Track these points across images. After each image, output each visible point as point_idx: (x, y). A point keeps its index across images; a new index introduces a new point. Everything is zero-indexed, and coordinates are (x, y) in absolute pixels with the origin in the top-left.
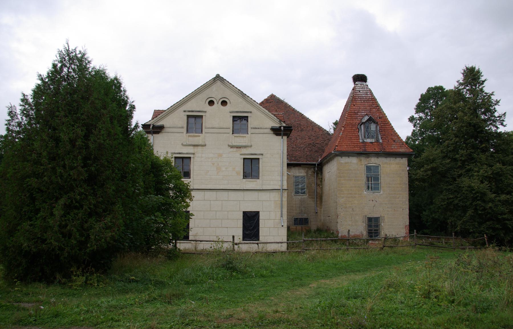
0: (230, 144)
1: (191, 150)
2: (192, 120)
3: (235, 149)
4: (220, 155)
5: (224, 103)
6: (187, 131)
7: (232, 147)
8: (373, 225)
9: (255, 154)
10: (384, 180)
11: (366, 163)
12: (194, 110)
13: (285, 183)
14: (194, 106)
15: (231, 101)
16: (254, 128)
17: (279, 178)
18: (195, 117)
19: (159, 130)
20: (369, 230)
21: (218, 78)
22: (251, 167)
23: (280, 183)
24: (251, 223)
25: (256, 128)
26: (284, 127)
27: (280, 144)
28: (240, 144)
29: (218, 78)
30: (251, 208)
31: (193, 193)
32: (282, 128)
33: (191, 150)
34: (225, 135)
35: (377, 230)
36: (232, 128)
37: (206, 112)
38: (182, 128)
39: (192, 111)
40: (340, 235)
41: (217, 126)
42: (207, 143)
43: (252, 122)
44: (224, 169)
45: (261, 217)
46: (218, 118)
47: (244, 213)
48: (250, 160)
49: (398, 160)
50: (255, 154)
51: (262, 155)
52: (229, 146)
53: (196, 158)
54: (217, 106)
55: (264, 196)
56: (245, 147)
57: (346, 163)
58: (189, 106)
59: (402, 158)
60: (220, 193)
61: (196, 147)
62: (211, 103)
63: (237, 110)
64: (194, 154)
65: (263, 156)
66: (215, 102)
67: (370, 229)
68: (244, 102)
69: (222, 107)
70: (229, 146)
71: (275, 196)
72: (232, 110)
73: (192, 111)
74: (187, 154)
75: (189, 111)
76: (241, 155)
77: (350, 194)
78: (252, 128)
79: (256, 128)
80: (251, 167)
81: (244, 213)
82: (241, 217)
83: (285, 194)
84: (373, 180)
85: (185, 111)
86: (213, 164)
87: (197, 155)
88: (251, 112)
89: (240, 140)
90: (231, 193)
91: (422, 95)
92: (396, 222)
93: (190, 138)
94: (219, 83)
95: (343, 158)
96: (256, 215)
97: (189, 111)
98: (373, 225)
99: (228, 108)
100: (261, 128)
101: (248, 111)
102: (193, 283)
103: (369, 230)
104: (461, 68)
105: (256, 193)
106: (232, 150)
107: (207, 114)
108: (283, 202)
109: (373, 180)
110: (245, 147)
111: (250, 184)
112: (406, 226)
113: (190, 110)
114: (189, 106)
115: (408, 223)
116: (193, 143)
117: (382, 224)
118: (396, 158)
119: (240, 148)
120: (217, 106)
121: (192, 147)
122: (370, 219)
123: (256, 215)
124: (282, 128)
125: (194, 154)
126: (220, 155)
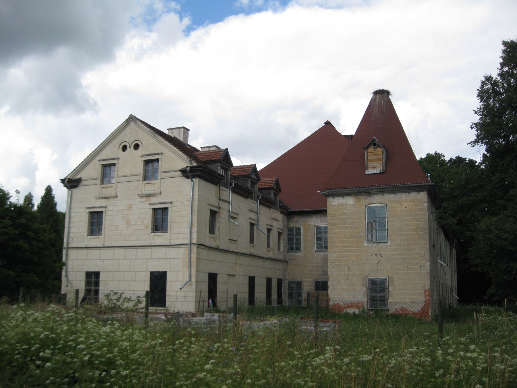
0: (140, 193)
1: (103, 203)
3: (144, 199)
4: (130, 207)
7: (142, 196)
8: (378, 290)
9: (164, 203)
11: (367, 202)
12: (108, 158)
13: (195, 236)
14: (107, 154)
15: (143, 143)
17: (188, 230)
19: (75, 184)
20: (372, 297)
21: (132, 119)
22: (160, 219)
23: (188, 237)
25: (166, 172)
28: (150, 192)
29: (132, 119)
30: (159, 268)
33: (103, 203)
34: (93, 187)
35: (384, 297)
37: (118, 159)
38: (97, 179)
39: (106, 160)
40: (331, 303)
42: (118, 194)
43: (163, 165)
44: (133, 222)
46: (131, 163)
47: (152, 273)
48: (161, 211)
49: (414, 195)
50: (164, 203)
52: (138, 195)
53: (107, 212)
54: (130, 150)
55: (173, 252)
56: (155, 195)
57: (339, 205)
58: (103, 155)
59: (418, 192)
60: (117, 251)
61: (108, 200)
62: (124, 148)
63: (148, 153)
65: (173, 205)
66: (128, 147)
67: (373, 294)
69: (134, 151)
70: (138, 195)
71: (183, 252)
73: (106, 160)
74: (100, 207)
75: (103, 160)
76: (150, 204)
79: (166, 172)
80: (160, 219)
81: (152, 273)
82: (148, 279)
84: (376, 224)
85: (100, 161)
86: (123, 217)
87: (108, 208)
88: (162, 154)
89: (150, 188)
90: (140, 251)
91: (488, 91)
92: (411, 287)
93: (104, 190)
94: (132, 124)
95: (336, 198)
96: (97, 275)
97: (103, 160)
98: (378, 290)
99: (140, 151)
100: (172, 171)
101: (159, 152)
103: (372, 297)
104: (501, 43)
105: (164, 250)
106: (142, 200)
107: (120, 161)
108: (192, 260)
109: (376, 224)
110: (155, 195)
111: (160, 238)
112: (425, 291)
113: (105, 158)
114: (103, 155)
115: (428, 286)
116: (106, 196)
117: (390, 289)
118: (409, 193)
119: (150, 197)
120: (130, 150)
121: (104, 200)
122: (373, 282)
123: (97, 275)
125: (106, 207)
126: (130, 207)
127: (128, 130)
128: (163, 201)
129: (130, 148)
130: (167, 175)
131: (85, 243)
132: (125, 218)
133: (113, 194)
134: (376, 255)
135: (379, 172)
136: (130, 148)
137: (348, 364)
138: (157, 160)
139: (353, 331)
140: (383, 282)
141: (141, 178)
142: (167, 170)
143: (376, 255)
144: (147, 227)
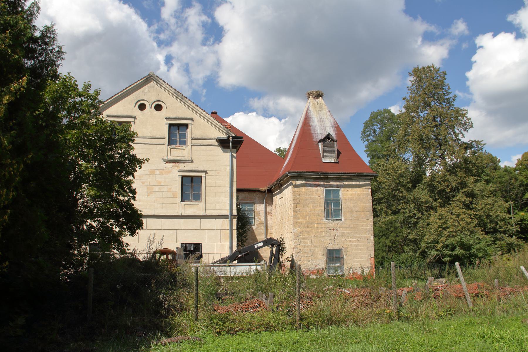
0: (166, 158)
2: (175, 131)
3: (171, 165)
5: (158, 108)
6: (169, 144)
7: (167, 161)
10: (344, 205)
15: (168, 105)
16: (196, 139)
18: (179, 126)
23: (228, 207)
24: (334, 256)
26: (233, 137)
27: (225, 158)
28: (178, 158)
31: (144, 220)
32: (231, 139)
36: (167, 138)
41: (149, 135)
45: (204, 251)
50: (198, 171)
51: (206, 172)
54: (149, 111)
56: (184, 162)
62: (142, 107)
63: (174, 116)
64: (206, 172)
68: (184, 107)
70: (164, 160)
72: (168, 116)
76: (179, 171)
77: (308, 222)
78: (193, 139)
83: (235, 221)
86: (143, 183)
89: (177, 153)
92: (360, 257)
99: (164, 113)
100: (205, 139)
102: (338, 323)
110: (184, 162)
111: (191, 208)
113: (115, 114)
117: (345, 257)
120: (149, 111)
124: (231, 139)
127: (146, 88)
128: (194, 169)
129: (151, 108)
130: (199, 142)
131: (176, 211)
132: (146, 184)
133: (188, 158)
134: (333, 229)
135: (333, 161)
136: (151, 108)
137: (510, 332)
138: (187, 126)
139: (323, 293)
140: (339, 251)
141: (166, 141)
142: (199, 137)
143: (333, 229)
144: (175, 195)
